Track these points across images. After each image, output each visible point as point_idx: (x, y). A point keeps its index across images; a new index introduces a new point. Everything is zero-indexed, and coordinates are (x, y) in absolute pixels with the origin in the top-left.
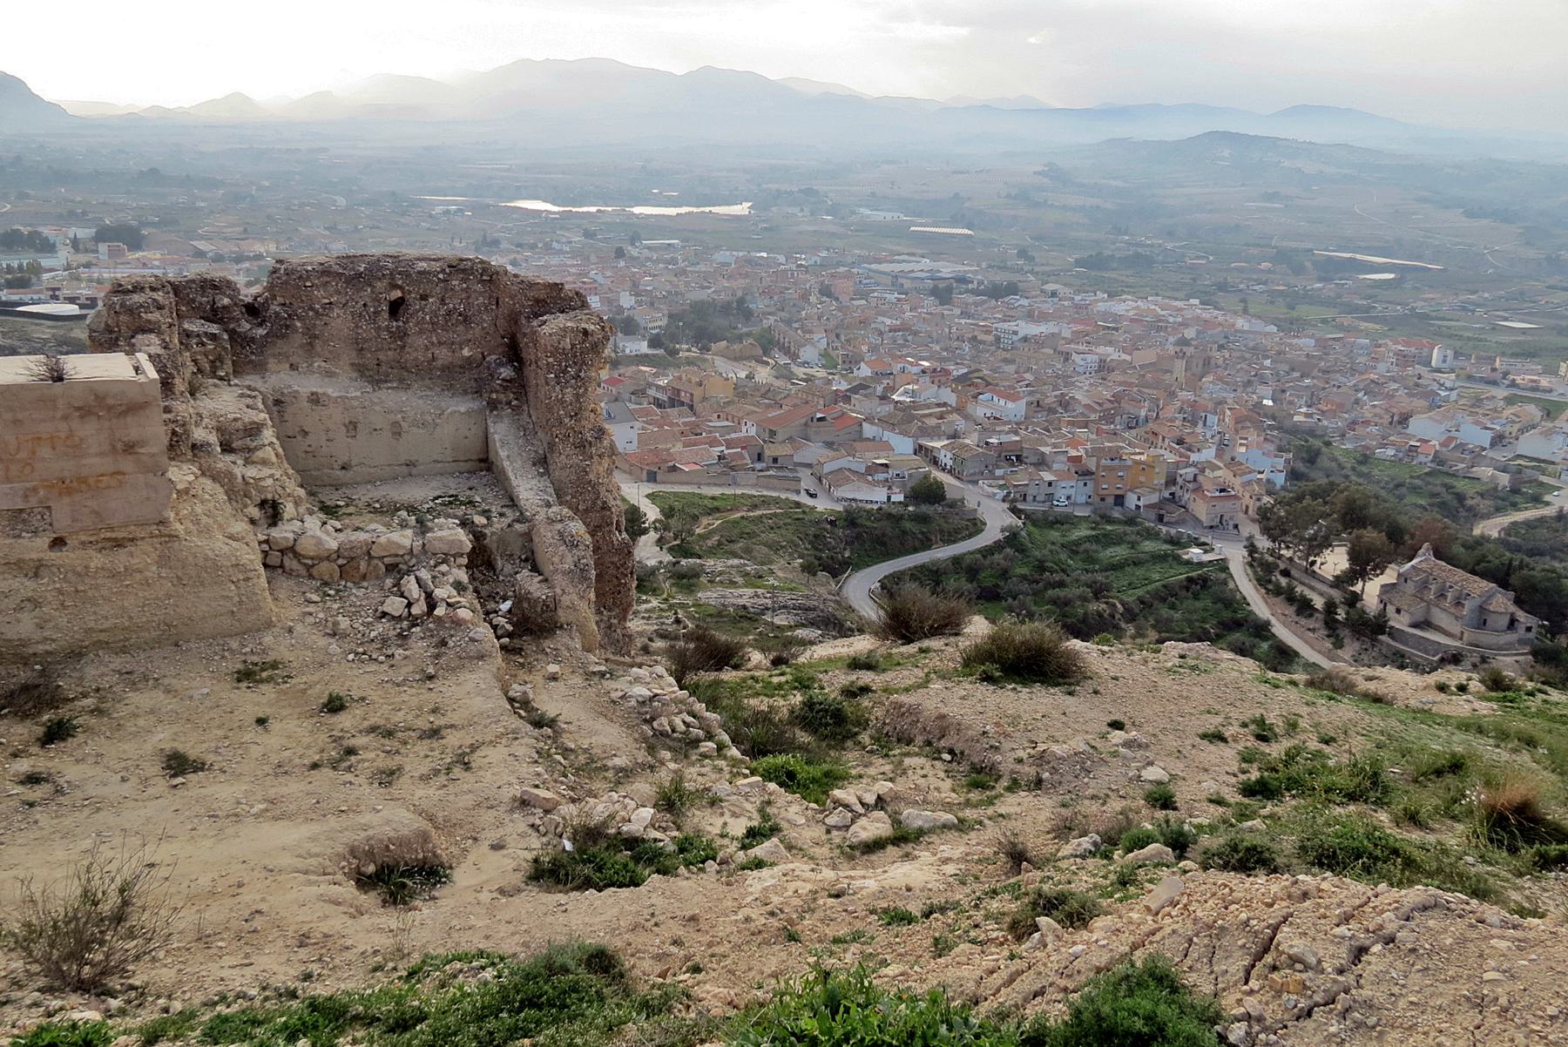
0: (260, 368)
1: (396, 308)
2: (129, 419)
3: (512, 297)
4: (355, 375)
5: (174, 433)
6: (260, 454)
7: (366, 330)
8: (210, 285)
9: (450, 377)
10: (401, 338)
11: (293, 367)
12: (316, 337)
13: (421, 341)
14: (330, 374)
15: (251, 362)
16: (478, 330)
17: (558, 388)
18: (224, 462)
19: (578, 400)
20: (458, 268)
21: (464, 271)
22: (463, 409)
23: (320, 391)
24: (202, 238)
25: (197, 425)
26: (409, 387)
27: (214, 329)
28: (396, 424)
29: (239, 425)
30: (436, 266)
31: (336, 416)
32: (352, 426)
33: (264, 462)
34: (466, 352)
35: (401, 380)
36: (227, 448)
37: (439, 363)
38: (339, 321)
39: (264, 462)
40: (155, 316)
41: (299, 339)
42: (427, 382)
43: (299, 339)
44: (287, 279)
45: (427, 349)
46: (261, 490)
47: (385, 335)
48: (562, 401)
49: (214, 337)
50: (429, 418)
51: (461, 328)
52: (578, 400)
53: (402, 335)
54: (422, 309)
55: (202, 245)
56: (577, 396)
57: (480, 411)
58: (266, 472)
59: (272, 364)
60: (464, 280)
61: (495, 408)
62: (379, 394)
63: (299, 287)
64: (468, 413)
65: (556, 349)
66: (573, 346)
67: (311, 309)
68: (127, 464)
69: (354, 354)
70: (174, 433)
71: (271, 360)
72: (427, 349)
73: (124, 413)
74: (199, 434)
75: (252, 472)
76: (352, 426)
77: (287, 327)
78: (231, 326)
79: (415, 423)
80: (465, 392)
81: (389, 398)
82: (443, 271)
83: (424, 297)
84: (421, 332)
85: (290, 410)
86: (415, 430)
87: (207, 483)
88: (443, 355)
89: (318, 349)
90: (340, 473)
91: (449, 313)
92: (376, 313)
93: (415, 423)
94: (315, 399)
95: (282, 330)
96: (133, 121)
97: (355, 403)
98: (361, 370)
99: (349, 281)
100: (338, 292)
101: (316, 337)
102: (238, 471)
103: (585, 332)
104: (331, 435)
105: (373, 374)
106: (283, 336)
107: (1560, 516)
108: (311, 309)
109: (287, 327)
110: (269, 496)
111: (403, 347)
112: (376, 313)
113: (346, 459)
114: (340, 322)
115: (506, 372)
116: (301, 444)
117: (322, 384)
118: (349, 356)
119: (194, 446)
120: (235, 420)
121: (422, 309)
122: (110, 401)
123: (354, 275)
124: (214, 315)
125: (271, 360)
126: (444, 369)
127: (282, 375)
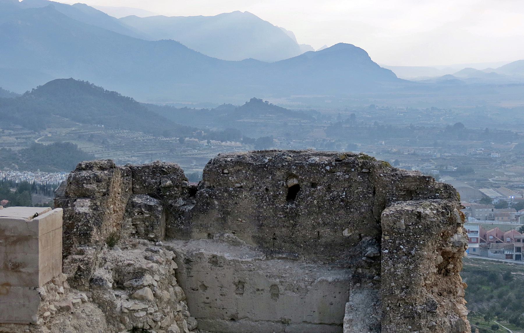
0: (186, 236)
1: (293, 193)
2: (18, 247)
3: (384, 187)
4: (255, 245)
5: (79, 268)
6: (140, 292)
7: (267, 210)
8: (158, 171)
9: (330, 253)
10: (293, 218)
11: (210, 236)
12: (228, 213)
13: (310, 222)
14: (235, 243)
15: (181, 230)
16: (356, 215)
17: (390, 262)
18: (110, 295)
19: (408, 275)
20: (344, 162)
21: (347, 164)
22: (330, 279)
23: (219, 254)
24: (492, 186)
25: (101, 266)
26: (295, 259)
27: (153, 202)
28: (274, 286)
29: (131, 269)
30: (325, 160)
31: (228, 276)
32: (240, 285)
33: (142, 299)
34: (346, 233)
35: (292, 252)
36: (119, 285)
37: (323, 240)
38: (246, 201)
39: (142, 299)
40: (93, 186)
41: (215, 214)
42: (313, 256)
43: (215, 214)
44: (216, 169)
45: (314, 227)
46: (134, 319)
47: (281, 215)
48: (393, 275)
49: (150, 208)
50: (302, 285)
51: (342, 212)
52: (408, 275)
53: (293, 215)
54: (311, 195)
55: (489, 193)
56: (408, 272)
57: (345, 282)
58: (141, 305)
59: (195, 232)
60: (347, 172)
61: (359, 281)
62: (270, 263)
63: (218, 174)
64: (335, 283)
65: (392, 228)
66: (407, 226)
67: (226, 191)
68: (13, 279)
69: (255, 229)
70: (79, 268)
71: (195, 230)
72: (314, 227)
73: (14, 243)
74: (99, 272)
75: (130, 305)
76: (240, 285)
77: (208, 204)
78: (169, 201)
79: (292, 288)
80: (342, 267)
81: (277, 266)
82: (330, 164)
83: (314, 185)
84: (310, 214)
85: (195, 268)
86: (289, 293)
87: (91, 307)
88: (327, 233)
89: (230, 223)
90: (230, 324)
91: (333, 199)
92: (275, 196)
93: (292, 288)
94: (215, 261)
95: (204, 208)
96: (449, 84)
97: (244, 266)
98: (260, 242)
99: (256, 169)
100: (246, 178)
101: (228, 213)
102: (118, 303)
103: (419, 215)
104: (225, 290)
105: (269, 247)
106: (205, 211)
107: (2, 169)
108: (226, 191)
109: (208, 204)
110: (140, 325)
111: (294, 225)
112: (275, 196)
113: (234, 312)
114: (246, 202)
115: (371, 251)
116: (201, 296)
117: (224, 252)
118: (252, 230)
119: (92, 280)
120: (129, 265)
121: (311, 195)
122: (7, 233)
123: (262, 166)
124: (157, 193)
125: (195, 230)
126: (327, 246)
127: (200, 241)
